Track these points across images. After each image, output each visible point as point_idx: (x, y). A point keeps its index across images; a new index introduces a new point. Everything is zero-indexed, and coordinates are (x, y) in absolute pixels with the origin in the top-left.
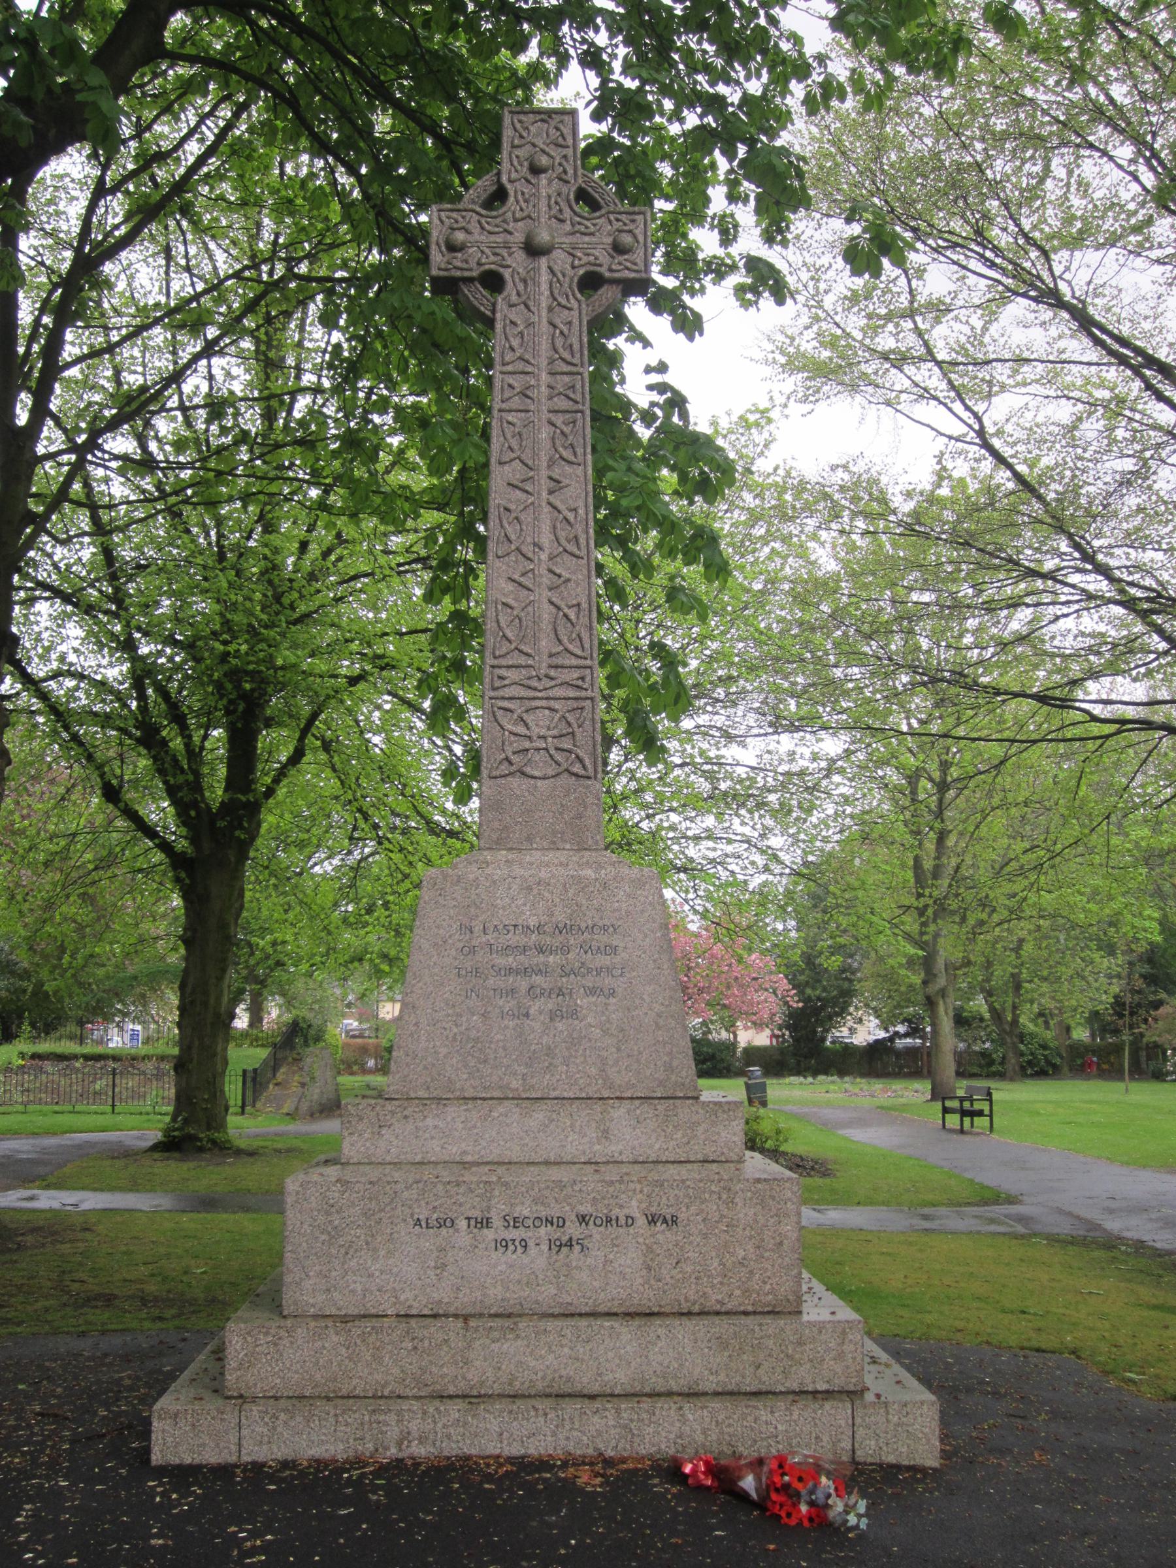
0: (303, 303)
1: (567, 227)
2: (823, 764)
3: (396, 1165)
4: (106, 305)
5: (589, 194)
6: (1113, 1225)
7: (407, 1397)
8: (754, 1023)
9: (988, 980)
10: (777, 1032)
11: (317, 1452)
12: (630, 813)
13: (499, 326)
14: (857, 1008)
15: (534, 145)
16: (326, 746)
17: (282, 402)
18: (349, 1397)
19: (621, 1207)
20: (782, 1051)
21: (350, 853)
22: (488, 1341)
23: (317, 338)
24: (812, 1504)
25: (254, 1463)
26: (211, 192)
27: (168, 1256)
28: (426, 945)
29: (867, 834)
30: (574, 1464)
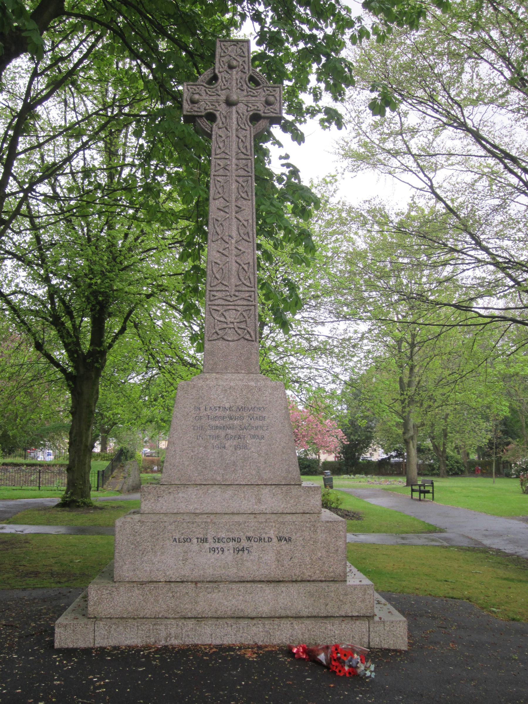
3: (166, 514)
6: (487, 542)
7: (169, 618)
8: (328, 451)
9: (432, 432)
11: (128, 642)
13: (214, 137)
14: (374, 445)
15: (230, 56)
16: (136, 326)
17: (117, 170)
18: (143, 618)
19: (266, 533)
20: (340, 464)
21: (146, 373)
22: (206, 593)
23: (132, 142)
24: (350, 666)
25: (101, 647)
28: (179, 416)
29: (379, 366)
30: (244, 648)
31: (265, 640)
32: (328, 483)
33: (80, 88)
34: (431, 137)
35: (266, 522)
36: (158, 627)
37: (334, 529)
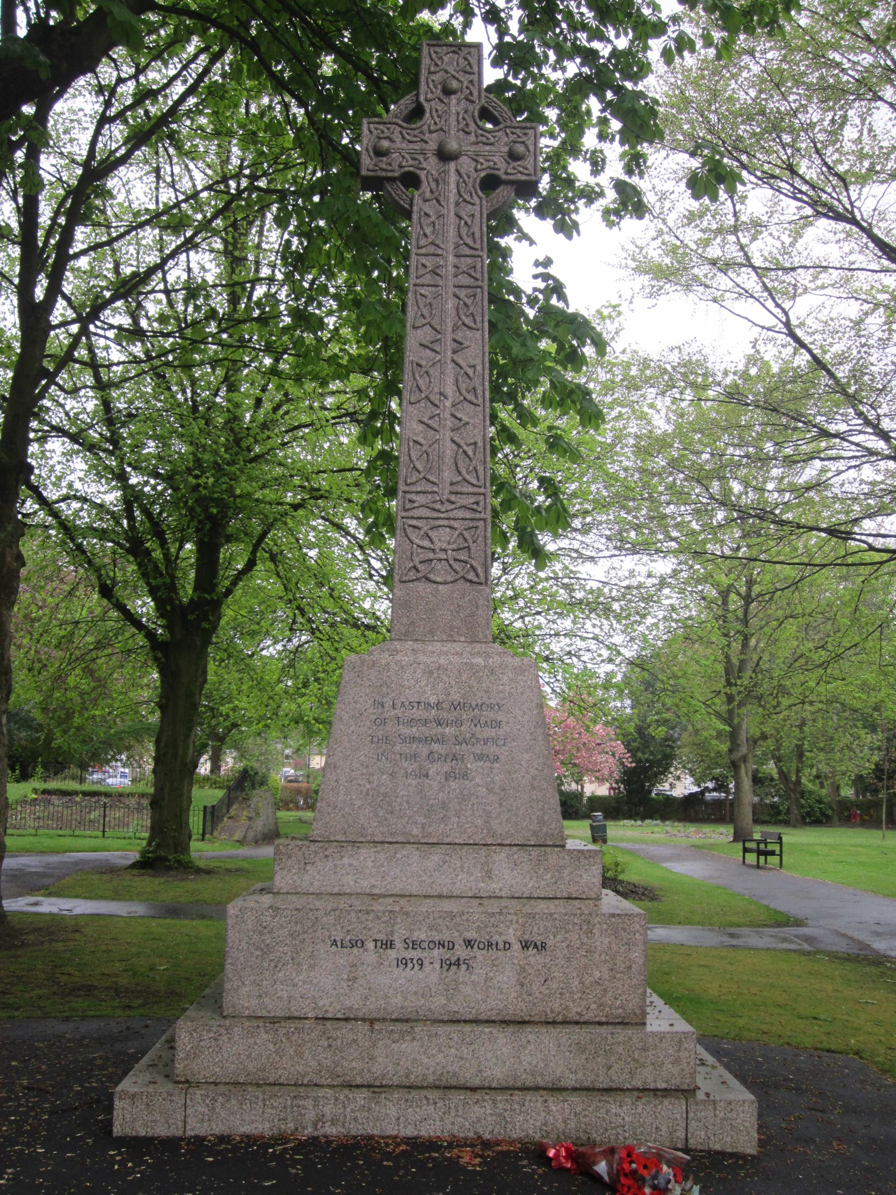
0: (262, 211)
1: (472, 138)
2: (655, 581)
4: (109, 213)
5: (490, 112)
6: (880, 945)
7: (322, 1086)
8: (597, 778)
9: (778, 749)
10: (615, 785)
11: (246, 1129)
12: (506, 615)
13: (415, 216)
14: (676, 769)
15: (447, 72)
16: (273, 558)
17: (244, 289)
18: (275, 1084)
19: (500, 934)
21: (290, 640)
22: (389, 1042)
23: (271, 237)
26: (192, 124)
27: (138, 954)
28: (346, 717)
29: (689, 635)
30: (458, 1146)
31: (496, 1130)
32: (599, 835)
33: (183, 145)
34: (787, 240)
35: (500, 913)
36: (301, 1103)
37: (624, 929)
